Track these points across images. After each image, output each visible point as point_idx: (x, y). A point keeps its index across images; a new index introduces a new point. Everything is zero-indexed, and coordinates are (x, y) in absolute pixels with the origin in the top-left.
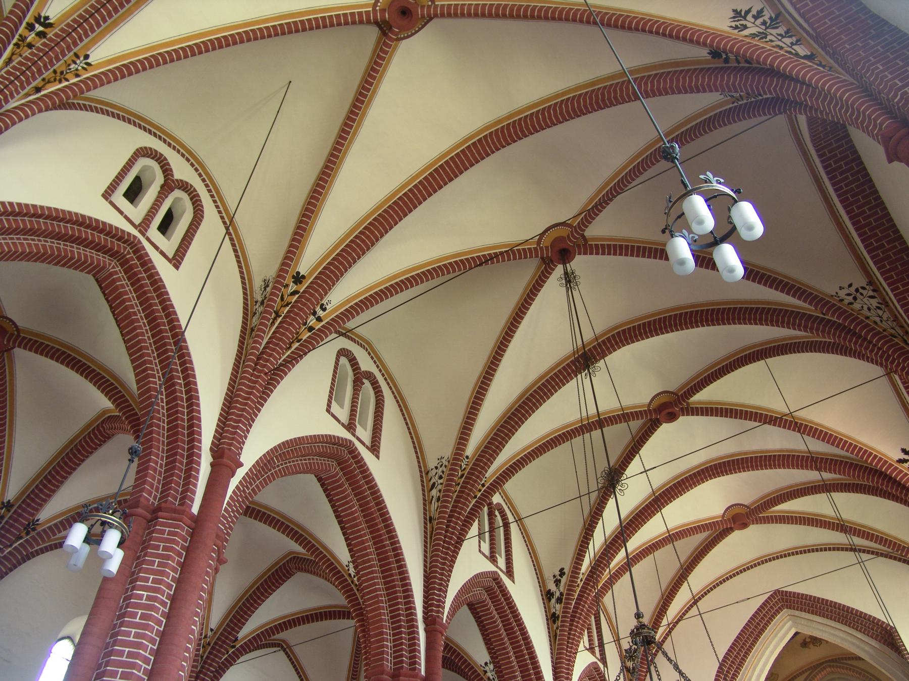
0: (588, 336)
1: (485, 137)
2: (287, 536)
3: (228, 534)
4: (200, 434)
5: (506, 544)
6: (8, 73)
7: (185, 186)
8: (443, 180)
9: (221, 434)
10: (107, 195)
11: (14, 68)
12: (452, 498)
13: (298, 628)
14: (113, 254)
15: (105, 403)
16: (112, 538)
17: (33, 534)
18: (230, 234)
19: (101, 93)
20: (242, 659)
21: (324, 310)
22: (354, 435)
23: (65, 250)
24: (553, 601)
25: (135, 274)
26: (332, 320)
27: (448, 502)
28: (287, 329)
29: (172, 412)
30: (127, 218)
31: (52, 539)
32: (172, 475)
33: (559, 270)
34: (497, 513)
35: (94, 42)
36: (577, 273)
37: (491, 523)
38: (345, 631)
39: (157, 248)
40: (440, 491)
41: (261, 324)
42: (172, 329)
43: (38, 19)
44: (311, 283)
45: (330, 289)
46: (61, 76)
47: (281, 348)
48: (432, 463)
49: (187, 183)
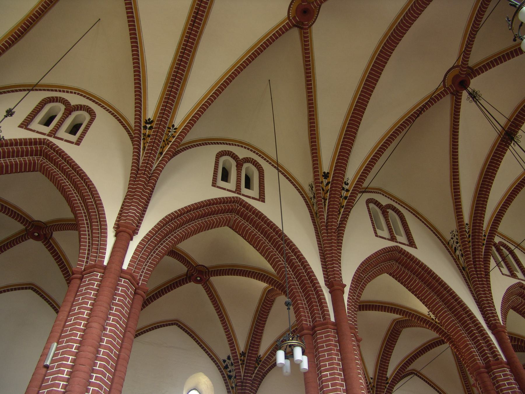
0: (503, 121)
1: (383, 47)
2: (388, 312)
3: (356, 325)
4: (316, 279)
5: (517, 263)
6: (146, 153)
7: (247, 160)
8: (373, 83)
9: (327, 275)
10: (214, 184)
11: (148, 150)
12: (470, 251)
13: (418, 360)
14: (231, 211)
15: (263, 285)
16: (298, 352)
17: (261, 363)
18: (280, 171)
19: (189, 138)
20: (395, 388)
21: (347, 184)
22: (397, 242)
23: (209, 221)
25: (246, 215)
26: (354, 187)
27: (468, 254)
28: (334, 204)
29: (298, 275)
30: (228, 190)
31: (270, 363)
32: (313, 306)
33: (465, 94)
34: (502, 248)
35: (173, 117)
36: (476, 90)
37: (501, 255)
38: (445, 351)
39: (249, 197)
40: (461, 250)
41: (319, 208)
42: (277, 233)
43: (146, 123)
44: (334, 174)
45: (345, 172)
46: (167, 141)
47: (336, 215)
48: (448, 237)
49: (247, 158)
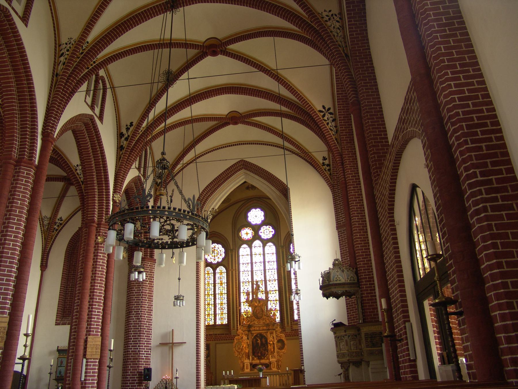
24: (123, 139)
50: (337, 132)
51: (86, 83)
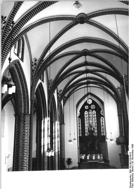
24: (59, 95)
50: (121, 95)
51: (56, 89)
